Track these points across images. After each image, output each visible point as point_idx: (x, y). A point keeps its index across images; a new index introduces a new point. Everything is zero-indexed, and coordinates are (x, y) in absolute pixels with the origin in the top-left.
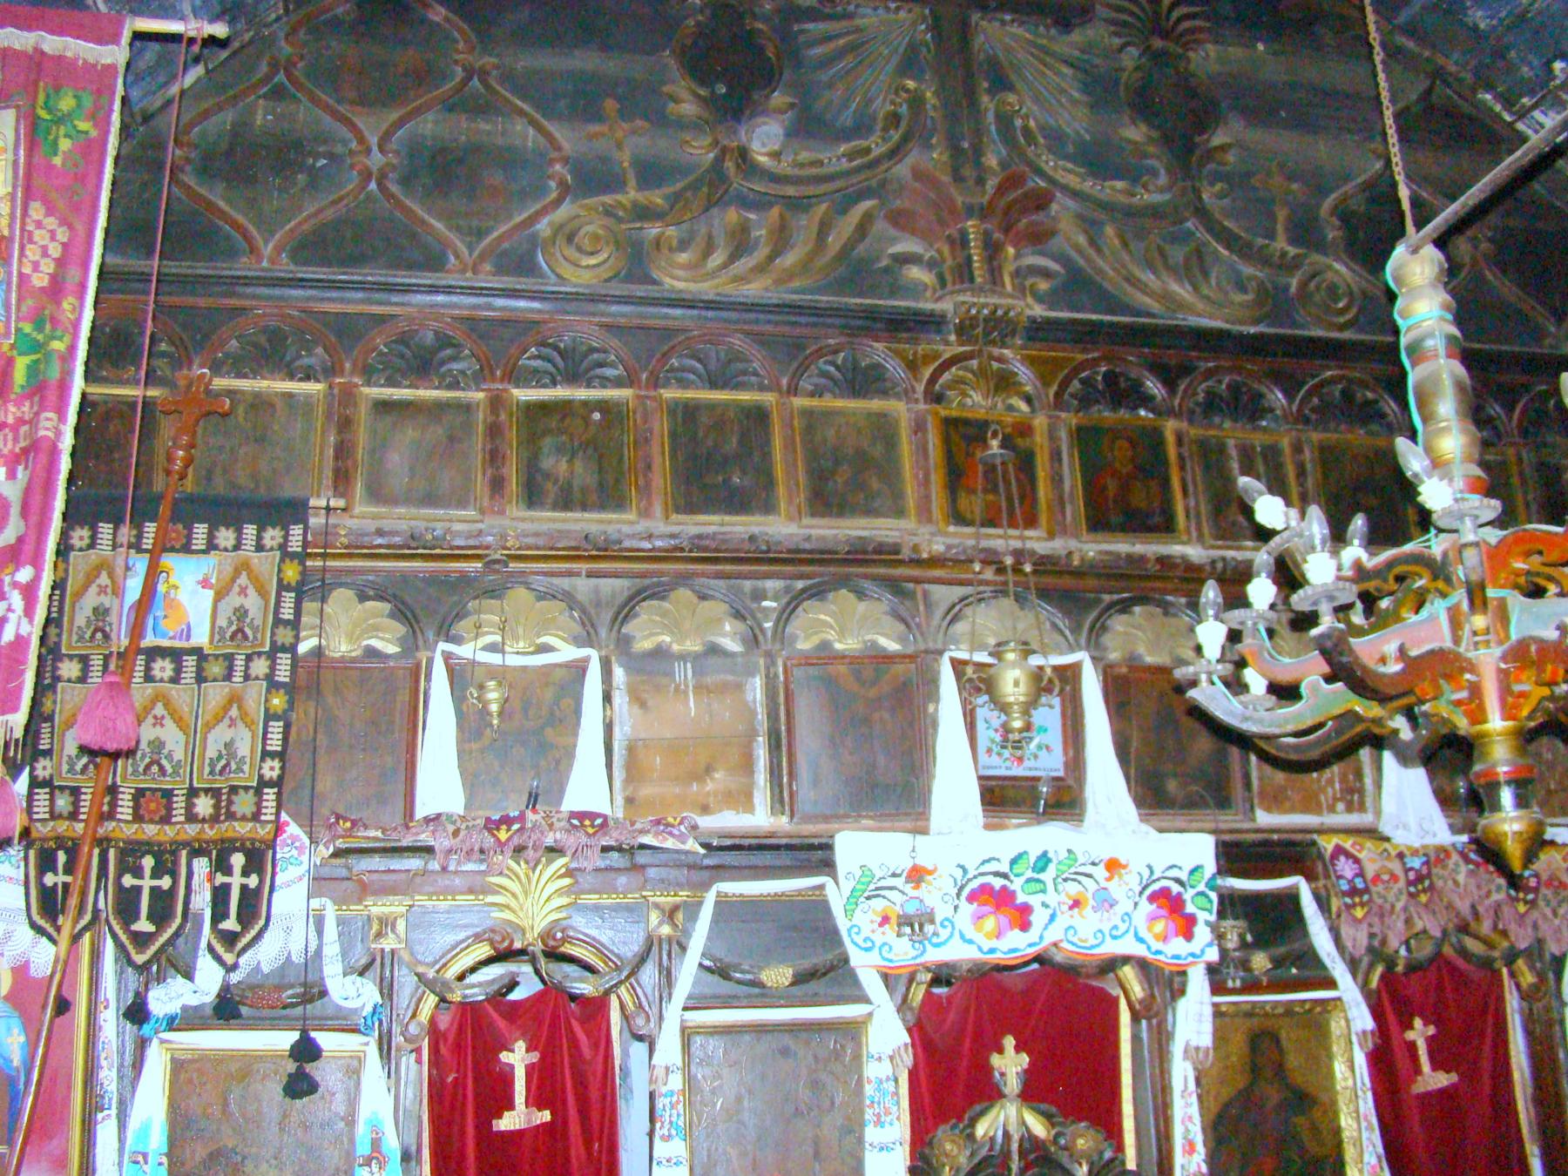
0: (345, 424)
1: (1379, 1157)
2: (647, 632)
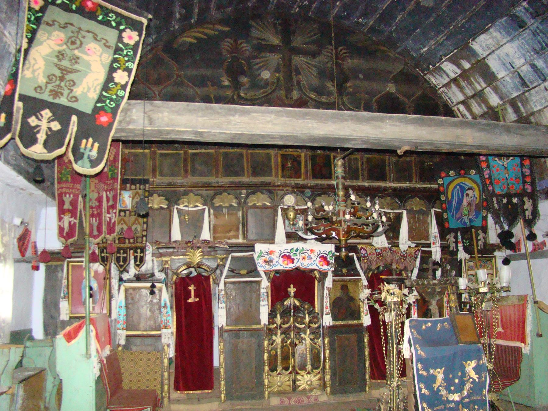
0: (154, 159)
2: (217, 202)
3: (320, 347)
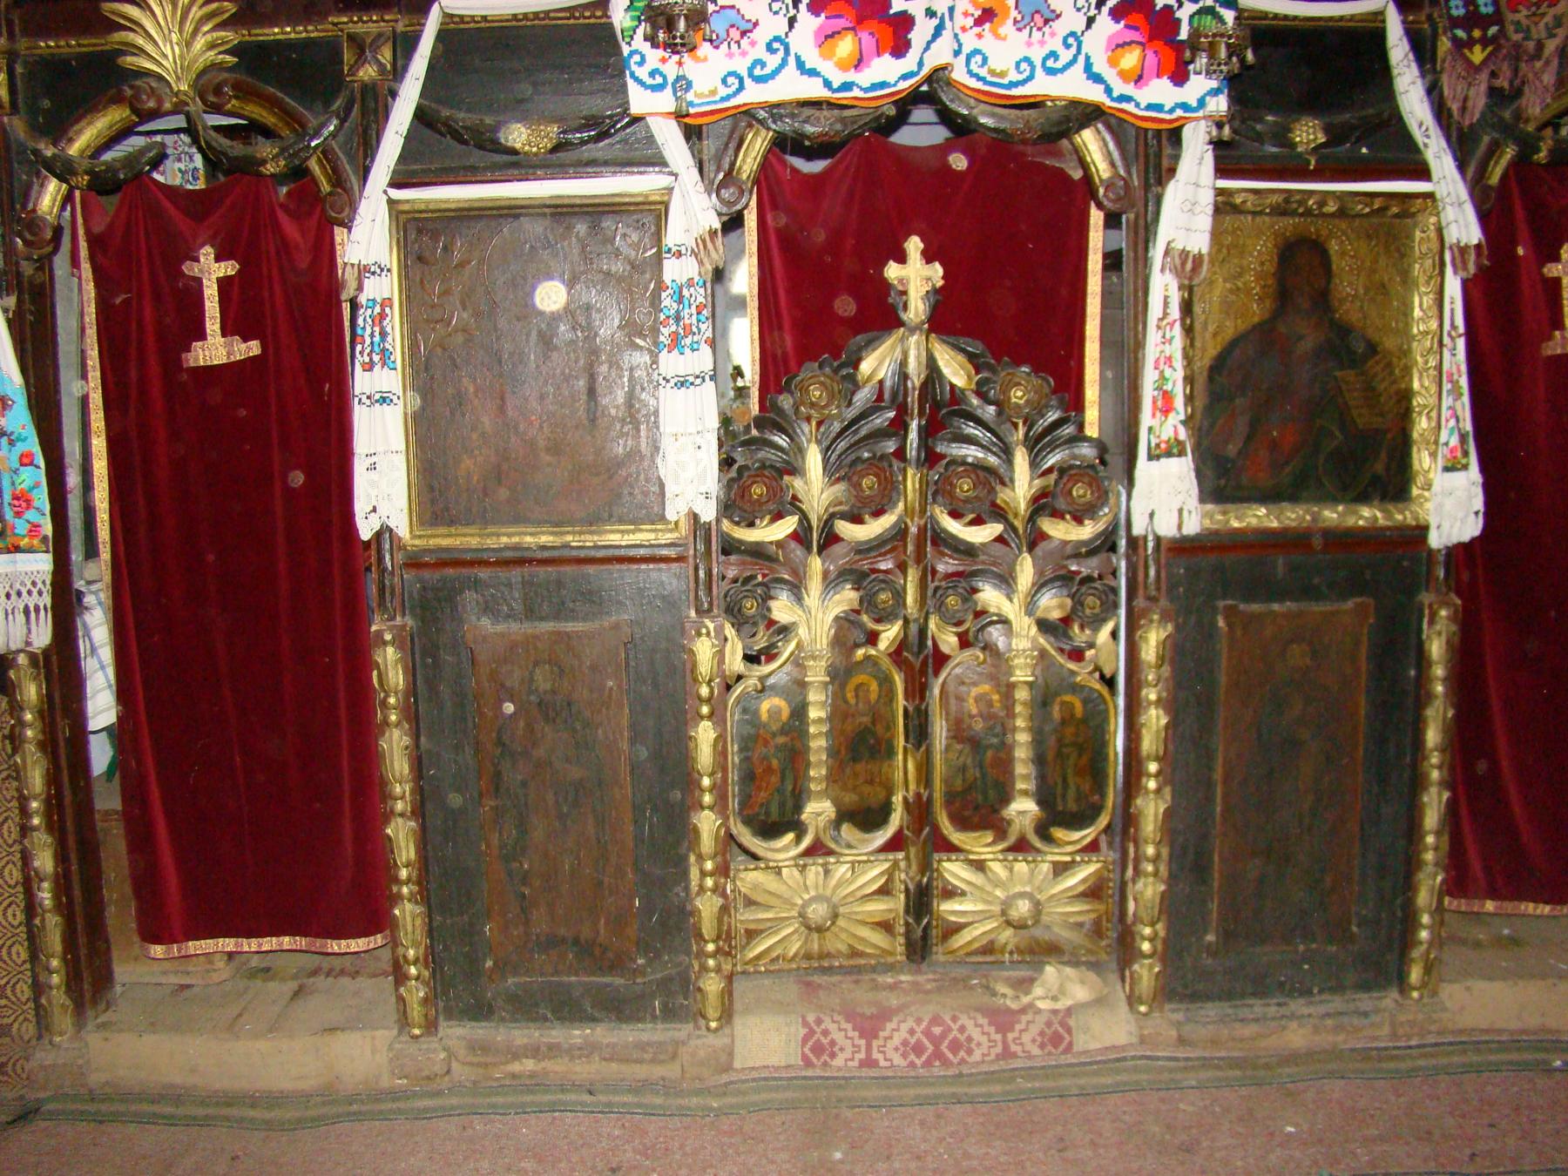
1: (1463, 438)
3: (1110, 682)
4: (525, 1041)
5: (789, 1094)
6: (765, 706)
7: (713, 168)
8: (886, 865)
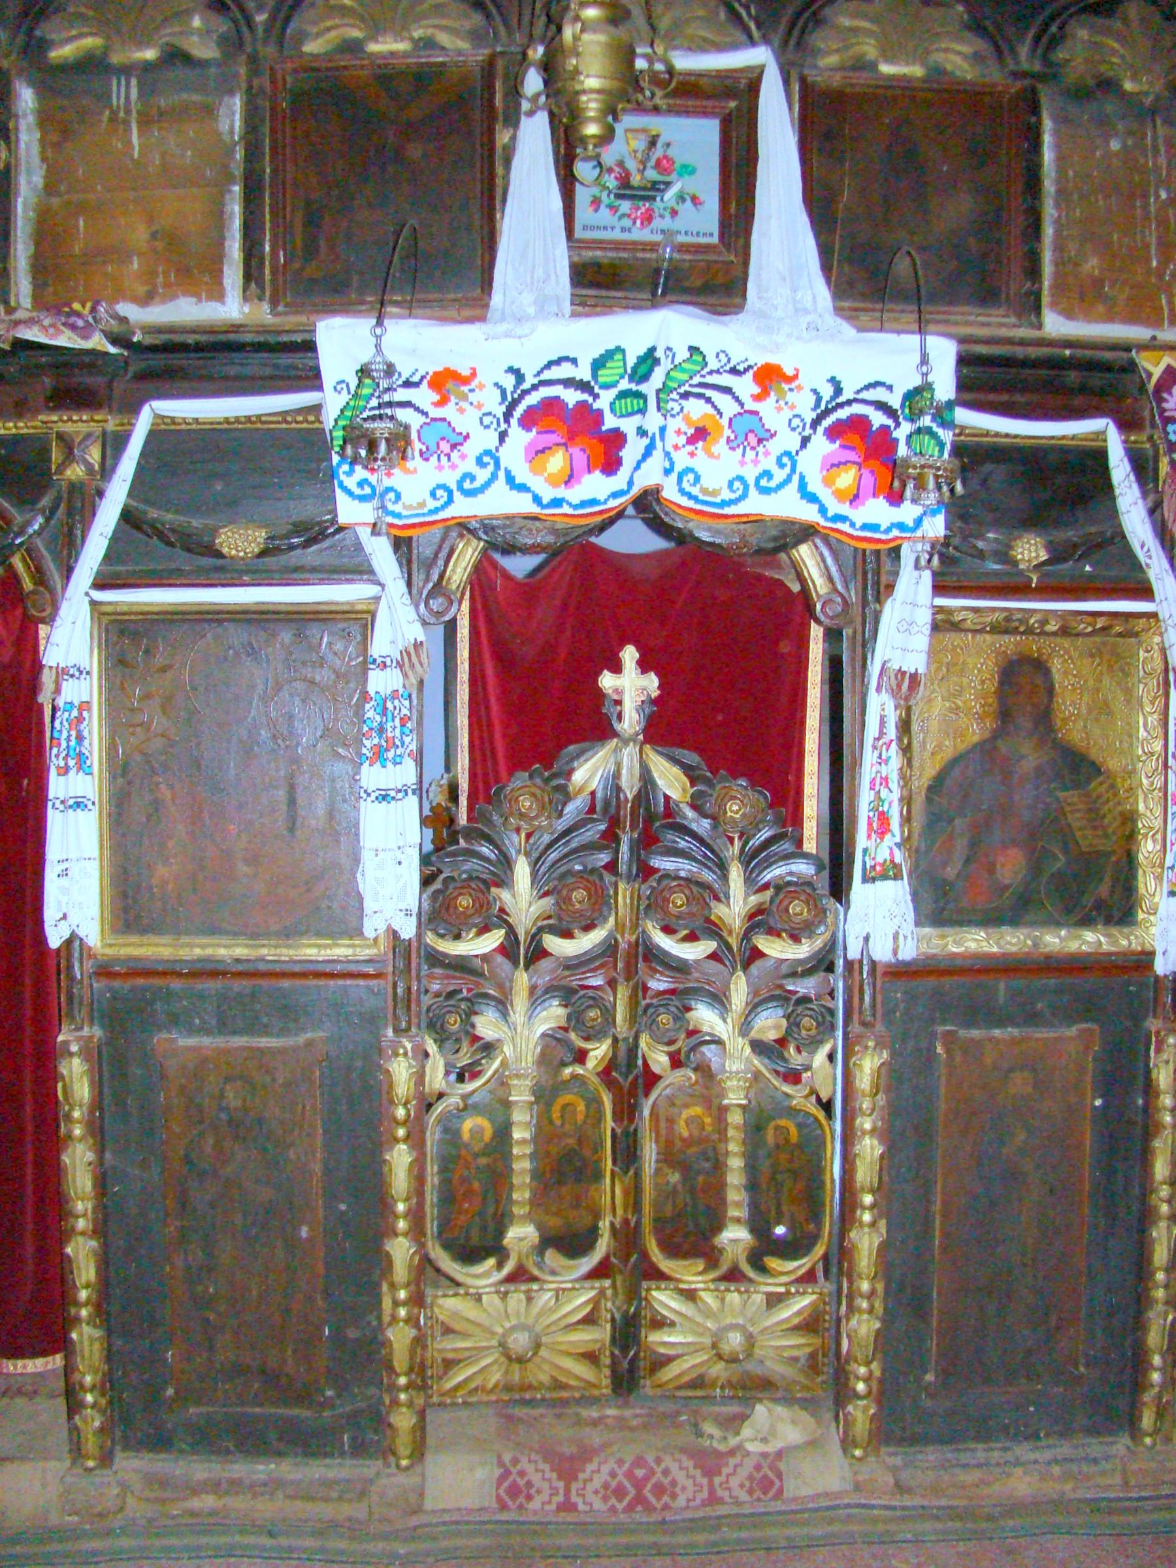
3: (827, 1107)
4: (206, 1475)
5: (481, 1541)
6: (468, 1125)
7: (422, 577)
8: (592, 1294)
